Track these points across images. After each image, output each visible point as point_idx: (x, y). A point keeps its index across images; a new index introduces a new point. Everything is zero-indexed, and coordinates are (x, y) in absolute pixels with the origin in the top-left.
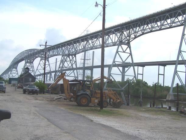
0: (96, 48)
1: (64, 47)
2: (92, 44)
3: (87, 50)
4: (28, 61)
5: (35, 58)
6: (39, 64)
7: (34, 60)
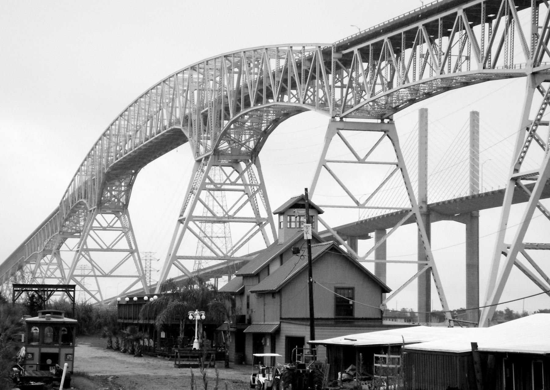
0: (429, 95)
1: (447, 34)
2: (114, 148)
3: (396, 109)
4: (217, 152)
5: (276, 122)
6: (323, 163)
7: (266, 133)
